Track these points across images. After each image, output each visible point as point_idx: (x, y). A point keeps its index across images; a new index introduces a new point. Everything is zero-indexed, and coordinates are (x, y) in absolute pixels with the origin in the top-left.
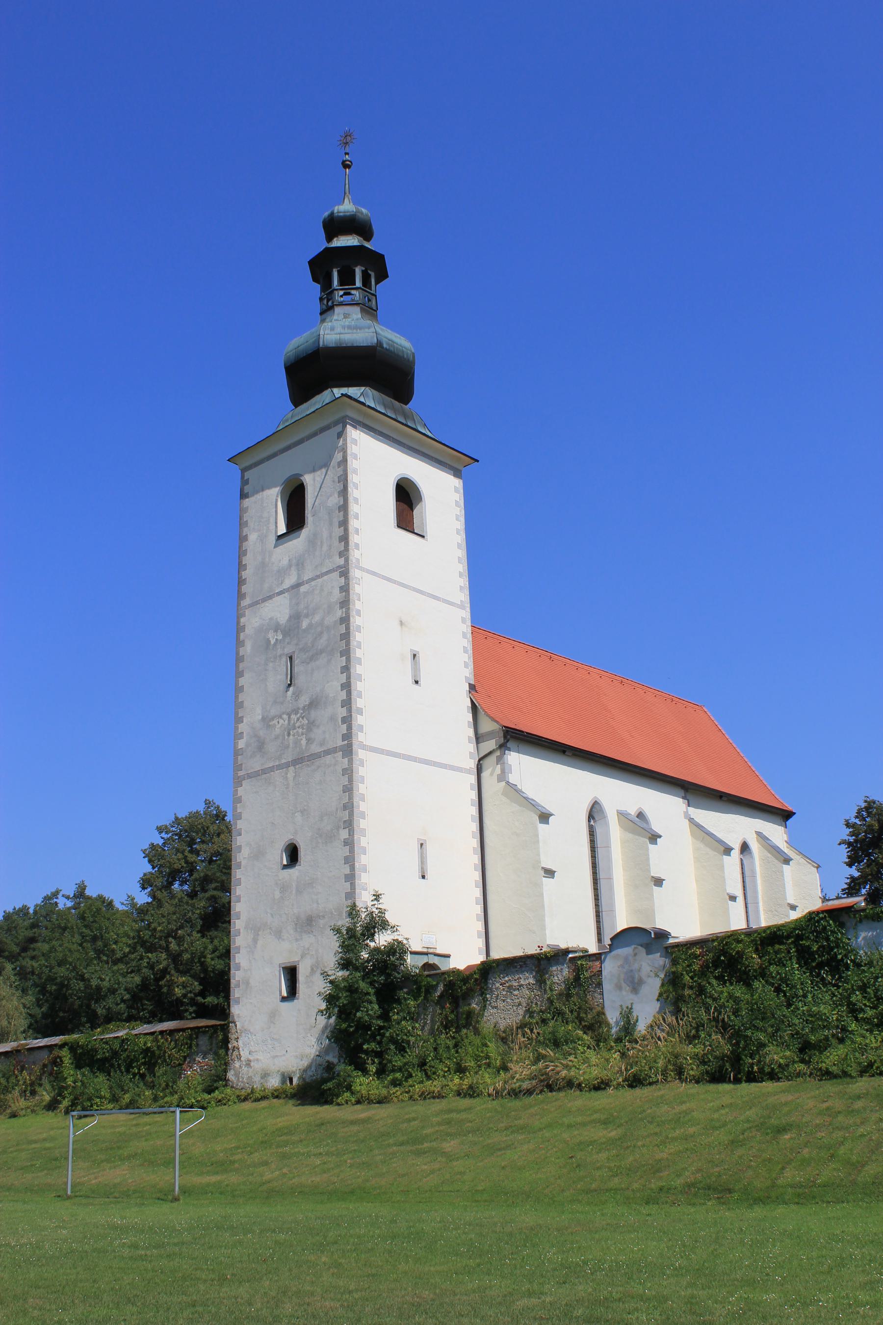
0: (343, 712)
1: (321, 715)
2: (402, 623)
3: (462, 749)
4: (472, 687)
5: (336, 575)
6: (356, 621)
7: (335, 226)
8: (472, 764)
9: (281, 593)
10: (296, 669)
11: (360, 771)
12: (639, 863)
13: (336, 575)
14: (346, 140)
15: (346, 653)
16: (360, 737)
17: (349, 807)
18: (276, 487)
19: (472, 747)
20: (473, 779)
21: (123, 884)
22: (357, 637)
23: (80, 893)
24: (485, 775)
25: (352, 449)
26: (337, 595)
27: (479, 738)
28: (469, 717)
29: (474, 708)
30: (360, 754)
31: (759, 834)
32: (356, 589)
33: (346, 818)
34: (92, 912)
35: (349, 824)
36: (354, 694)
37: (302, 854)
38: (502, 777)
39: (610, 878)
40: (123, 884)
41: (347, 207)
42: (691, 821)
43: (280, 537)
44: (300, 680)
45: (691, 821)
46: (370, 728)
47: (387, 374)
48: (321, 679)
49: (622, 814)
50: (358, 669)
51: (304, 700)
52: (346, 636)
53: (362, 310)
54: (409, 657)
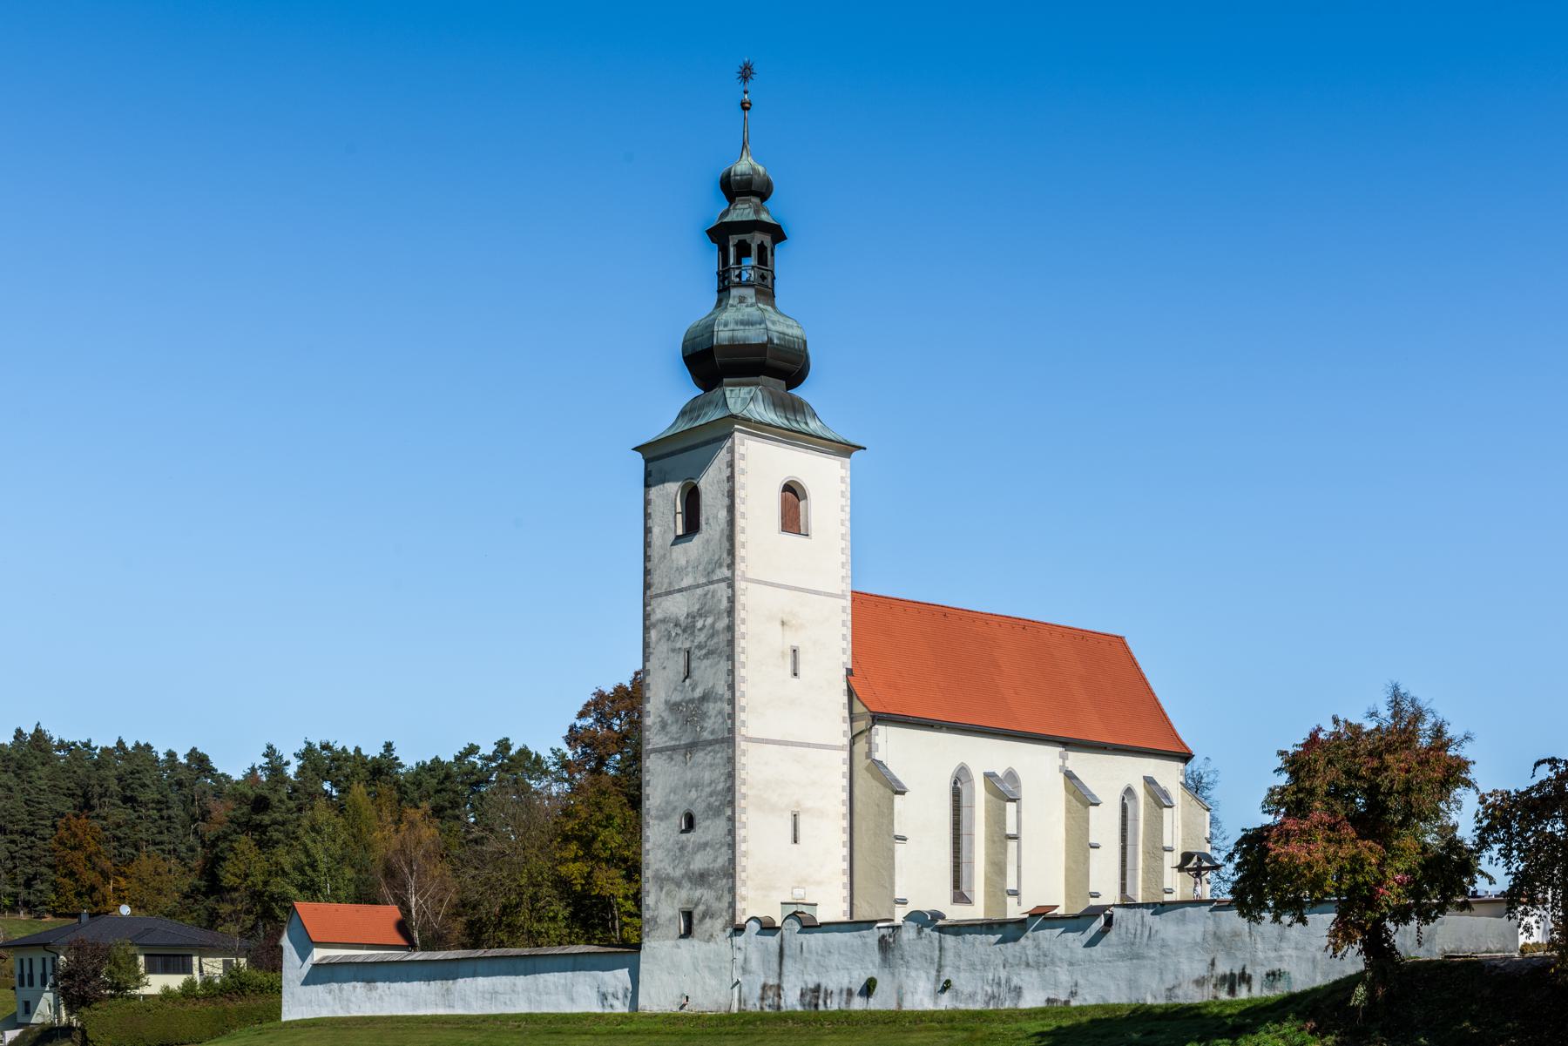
0: (727, 708)
1: (712, 708)
2: (783, 623)
3: (836, 728)
4: (850, 672)
5: (724, 585)
6: (740, 629)
7: (733, 188)
8: (846, 741)
9: (680, 591)
10: (693, 665)
11: (741, 760)
12: (996, 820)
13: (724, 585)
14: (746, 73)
15: (731, 657)
16: (742, 731)
17: (731, 790)
18: (676, 480)
19: (846, 726)
20: (846, 754)
21: (546, 737)
22: (740, 644)
23: (504, 745)
24: (856, 747)
25: (739, 449)
26: (725, 604)
27: (852, 718)
28: (845, 699)
29: (851, 693)
30: (741, 745)
31: (1149, 781)
32: (741, 599)
33: (727, 799)
34: (516, 764)
35: (732, 803)
36: (738, 694)
37: (697, 821)
38: (869, 754)
39: (971, 834)
40: (546, 737)
41: (743, 166)
42: (1069, 776)
43: (678, 537)
44: (696, 675)
45: (1069, 776)
46: (750, 723)
47: (781, 367)
48: (709, 675)
49: (989, 776)
50: (740, 672)
51: (698, 693)
52: (731, 643)
53: (758, 292)
54: (790, 652)
